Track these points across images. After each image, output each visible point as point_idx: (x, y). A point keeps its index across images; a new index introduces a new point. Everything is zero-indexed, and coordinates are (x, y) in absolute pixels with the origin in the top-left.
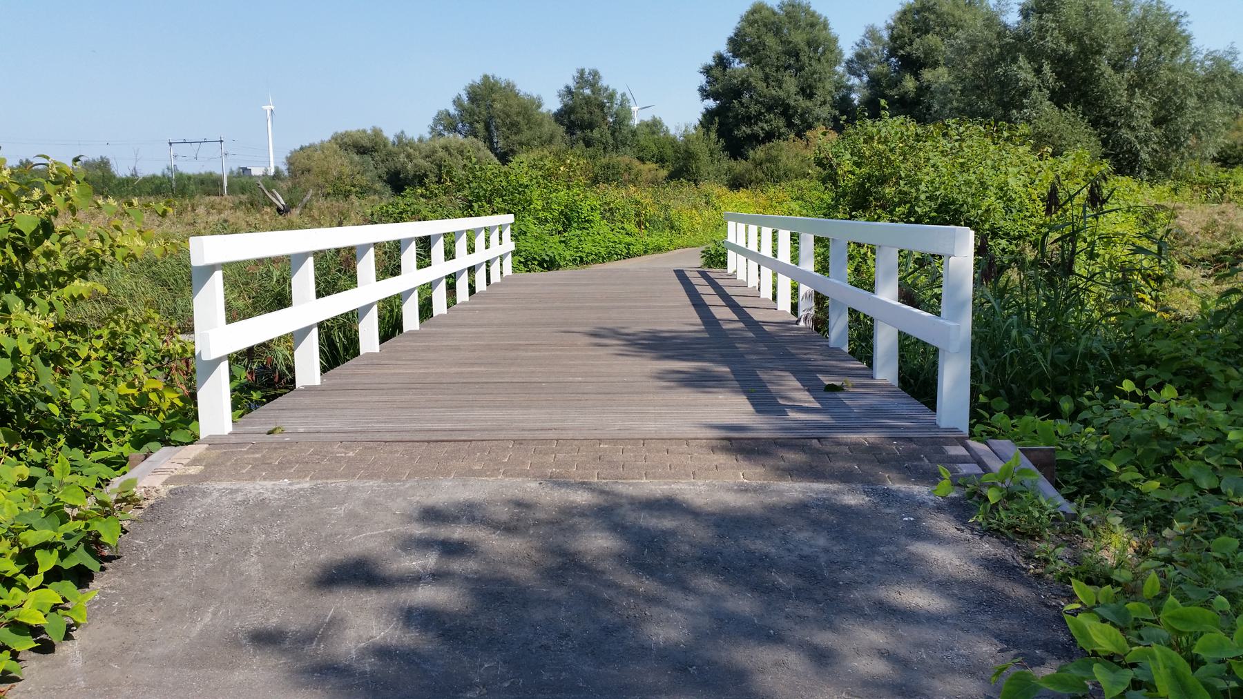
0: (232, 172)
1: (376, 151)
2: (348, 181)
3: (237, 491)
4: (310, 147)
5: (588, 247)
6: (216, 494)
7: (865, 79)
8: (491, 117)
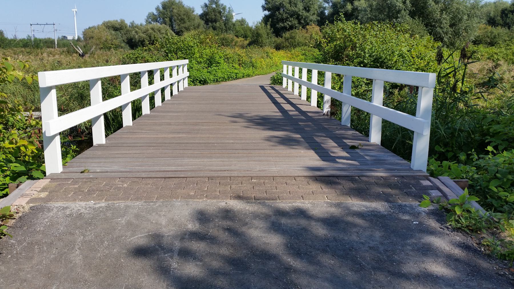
0: (59, 38)
1: (122, 29)
2: (110, 42)
3: (67, 208)
4: (93, 27)
5: (220, 75)
6: (55, 210)
7: (331, 4)
8: (172, 16)
